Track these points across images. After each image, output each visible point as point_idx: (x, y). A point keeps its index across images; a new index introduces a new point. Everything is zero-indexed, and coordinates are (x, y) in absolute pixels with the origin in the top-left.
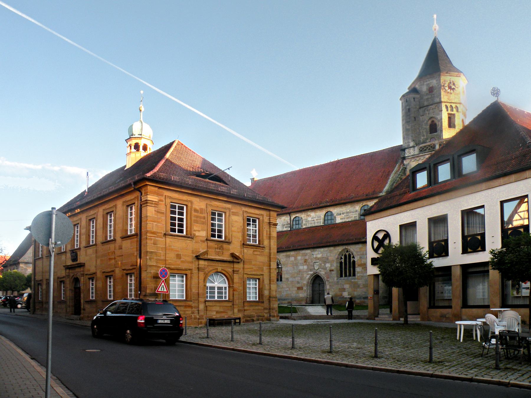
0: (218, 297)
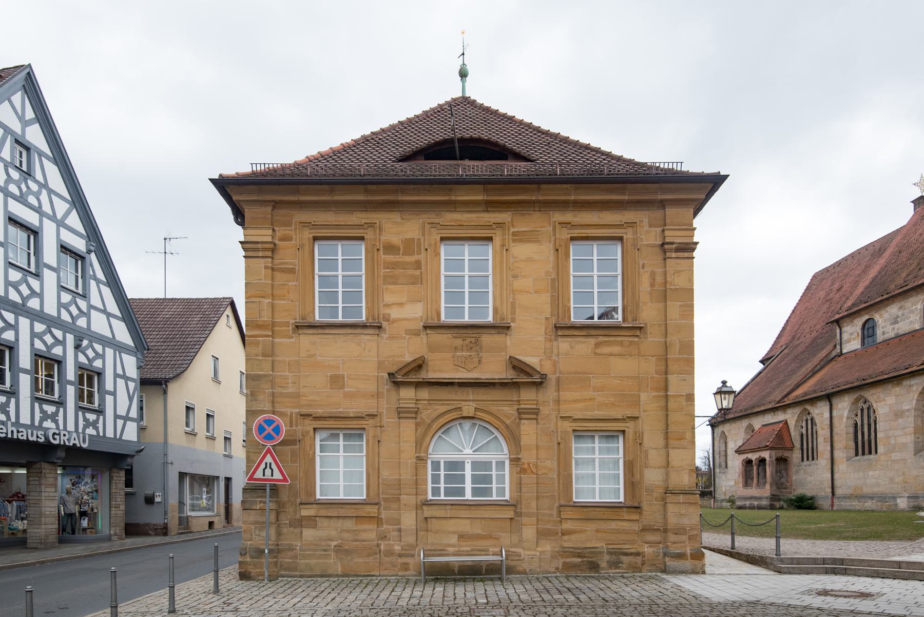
0: (475, 492)
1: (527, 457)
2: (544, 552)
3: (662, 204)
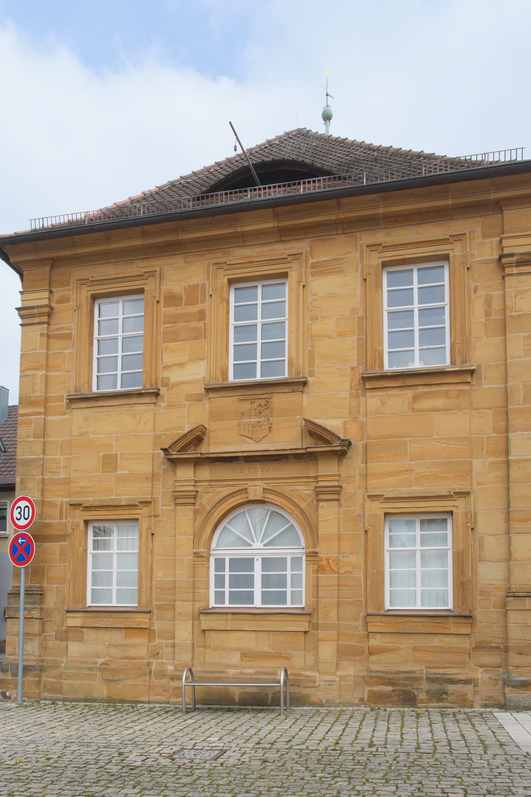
0: (266, 597)
1: (326, 550)
2: (345, 676)
3: (498, 206)
